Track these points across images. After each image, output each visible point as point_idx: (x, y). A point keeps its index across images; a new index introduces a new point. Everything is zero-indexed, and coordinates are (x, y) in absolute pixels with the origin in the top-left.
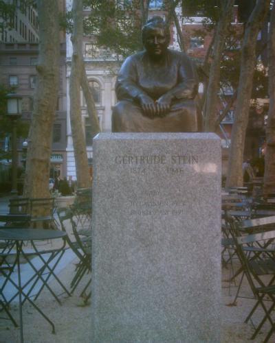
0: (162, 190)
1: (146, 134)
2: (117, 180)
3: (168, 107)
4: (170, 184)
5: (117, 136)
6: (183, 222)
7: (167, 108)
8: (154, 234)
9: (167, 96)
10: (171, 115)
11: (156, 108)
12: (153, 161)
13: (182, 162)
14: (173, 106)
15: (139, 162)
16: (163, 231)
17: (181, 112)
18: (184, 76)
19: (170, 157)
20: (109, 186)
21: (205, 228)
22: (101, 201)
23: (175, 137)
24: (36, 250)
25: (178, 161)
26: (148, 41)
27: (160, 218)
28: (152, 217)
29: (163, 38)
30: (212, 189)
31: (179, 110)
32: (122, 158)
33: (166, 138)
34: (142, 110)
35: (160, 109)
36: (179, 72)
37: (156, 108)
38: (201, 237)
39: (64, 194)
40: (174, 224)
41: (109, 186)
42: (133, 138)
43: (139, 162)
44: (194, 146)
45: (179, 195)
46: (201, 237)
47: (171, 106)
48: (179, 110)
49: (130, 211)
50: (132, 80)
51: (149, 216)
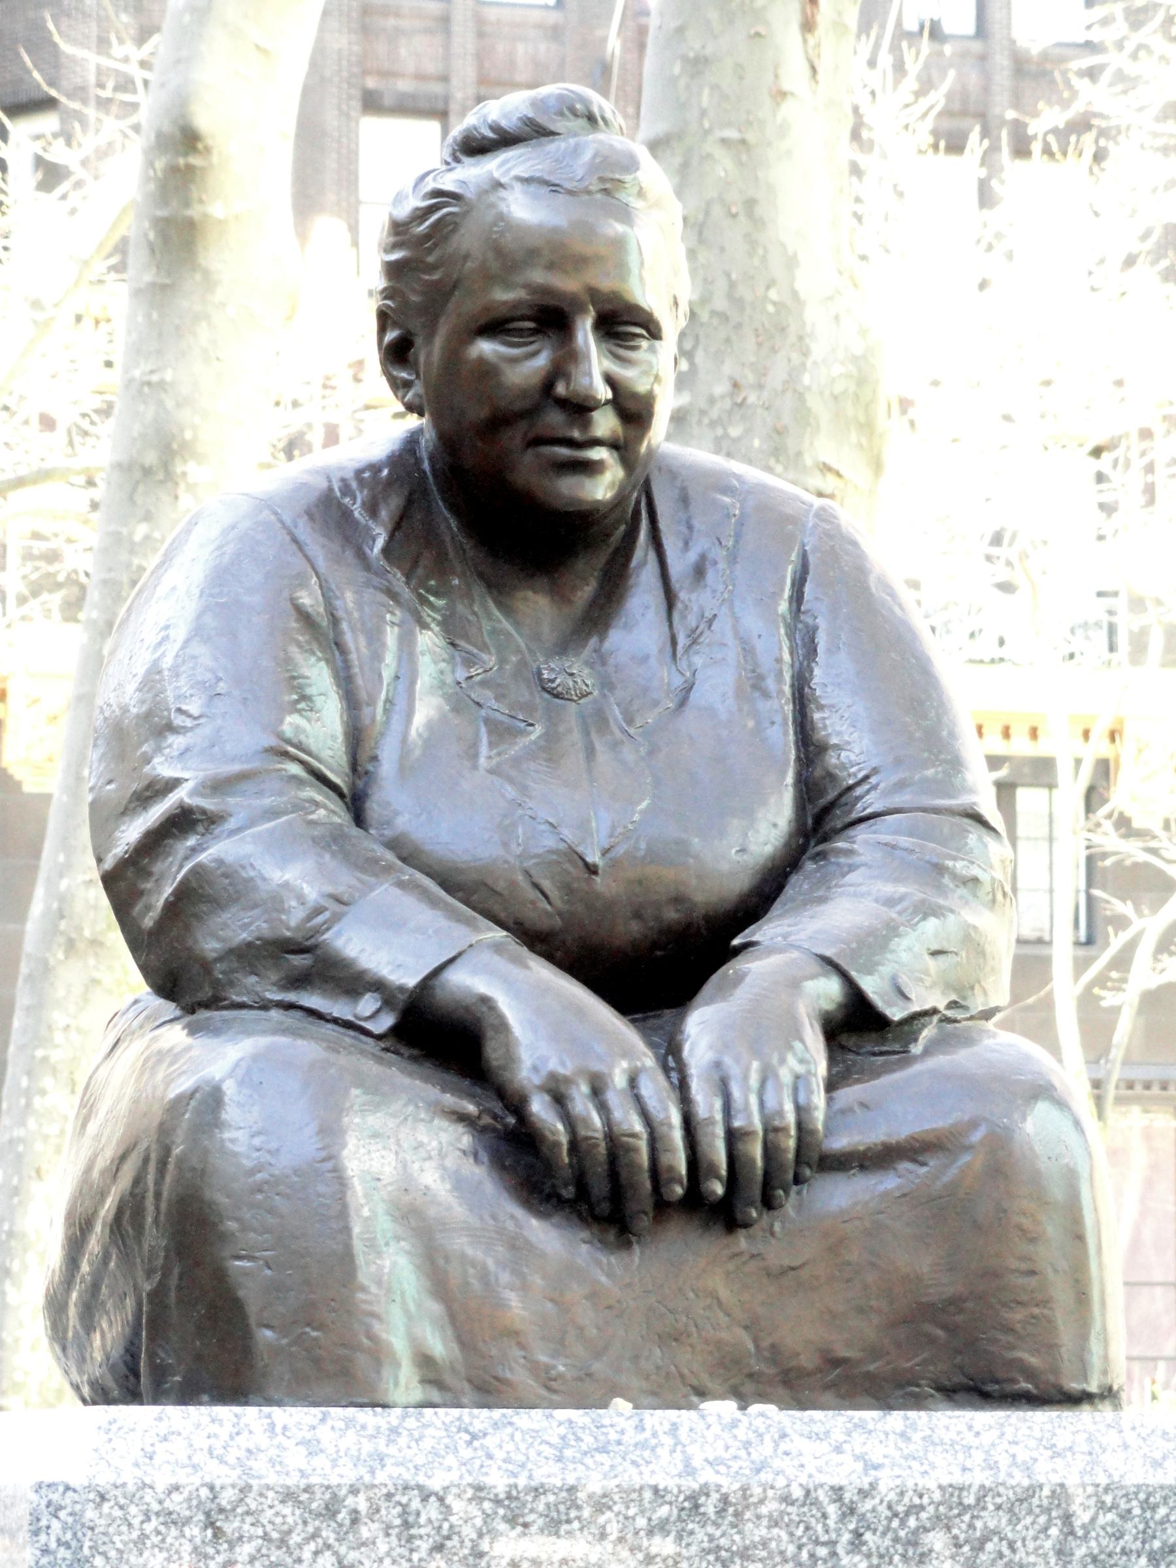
26: (486, 348)
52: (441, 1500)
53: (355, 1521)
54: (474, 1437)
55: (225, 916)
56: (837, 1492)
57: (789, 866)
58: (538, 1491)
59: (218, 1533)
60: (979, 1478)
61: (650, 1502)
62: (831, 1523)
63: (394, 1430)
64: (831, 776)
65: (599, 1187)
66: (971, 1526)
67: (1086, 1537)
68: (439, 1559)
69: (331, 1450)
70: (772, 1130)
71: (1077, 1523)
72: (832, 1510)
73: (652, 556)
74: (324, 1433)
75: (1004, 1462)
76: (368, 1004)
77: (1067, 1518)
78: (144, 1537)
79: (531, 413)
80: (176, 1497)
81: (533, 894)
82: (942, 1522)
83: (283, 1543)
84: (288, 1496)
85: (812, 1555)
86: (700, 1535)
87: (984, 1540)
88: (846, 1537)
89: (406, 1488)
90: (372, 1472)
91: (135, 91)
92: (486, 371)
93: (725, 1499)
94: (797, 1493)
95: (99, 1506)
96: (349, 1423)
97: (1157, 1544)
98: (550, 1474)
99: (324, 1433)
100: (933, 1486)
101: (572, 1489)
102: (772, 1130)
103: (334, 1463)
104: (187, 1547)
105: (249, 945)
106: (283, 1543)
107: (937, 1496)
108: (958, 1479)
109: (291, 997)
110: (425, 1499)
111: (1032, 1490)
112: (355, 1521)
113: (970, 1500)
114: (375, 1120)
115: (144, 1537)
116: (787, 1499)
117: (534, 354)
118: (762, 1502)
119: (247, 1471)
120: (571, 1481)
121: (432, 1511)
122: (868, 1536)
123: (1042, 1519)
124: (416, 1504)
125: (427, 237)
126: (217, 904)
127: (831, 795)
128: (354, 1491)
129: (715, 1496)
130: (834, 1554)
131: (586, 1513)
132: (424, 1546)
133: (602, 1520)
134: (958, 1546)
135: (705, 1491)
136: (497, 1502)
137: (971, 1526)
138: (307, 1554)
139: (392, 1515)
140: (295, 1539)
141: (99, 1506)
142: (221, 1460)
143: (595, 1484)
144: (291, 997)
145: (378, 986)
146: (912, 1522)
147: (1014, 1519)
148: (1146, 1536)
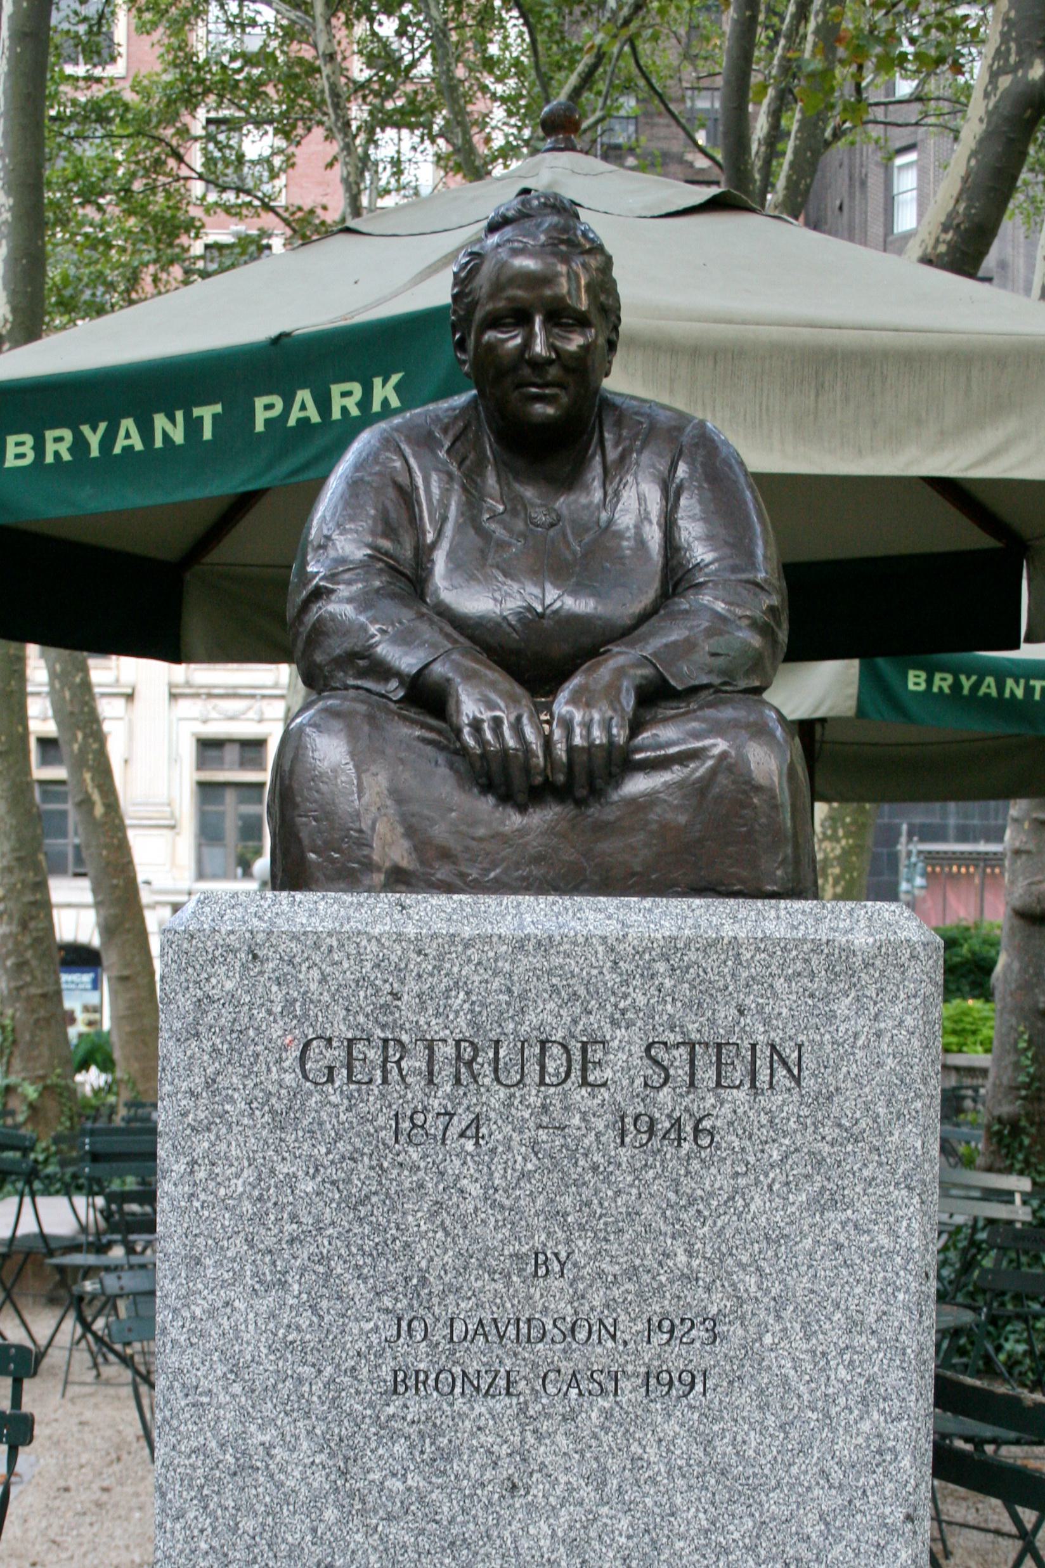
0: (583, 1245)
1: (489, 902)
2: (310, 1186)
3: (620, 734)
4: (633, 1214)
5: (626, 511)
6: (708, 1444)
7: (611, 742)
8: (530, 1507)
9: (605, 671)
10: (638, 785)
11: (548, 742)
12: (533, 1069)
13: (706, 1076)
14: (645, 736)
15: (445, 1074)
16: (587, 1493)
17: (699, 769)
18: (701, 553)
19: (638, 1050)
20: (259, 1218)
21: (837, 1475)
22: (212, 1313)
23: (668, 928)
24: (13, 1285)
25: (680, 1073)
26: (490, 336)
27: (568, 1418)
28: (523, 1409)
29: (582, 322)
30: (884, 1240)
31: (683, 758)
32: (337, 1054)
33: (612, 928)
34: (463, 751)
35: (571, 749)
36: (669, 526)
37: (548, 742)
38: (814, 1531)
39: (341, 534)
40: (652, 1453)
41: (259, 1218)
42: (411, 930)
43: (445, 1074)
44: (780, 984)
45: (689, 1278)
46: (814, 1531)
47: (636, 727)
48: (683, 758)
49: (386, 1372)
50: (395, 571)
51: (500, 1404)
52: (378, 940)
53: (330, 951)
54: (404, 908)
55: (331, 641)
56: (604, 939)
58: (434, 936)
59: (255, 957)
62: (600, 956)
63: (361, 905)
64: (681, 565)
66: (681, 960)
67: (749, 967)
69: (322, 913)
71: (744, 959)
72: (600, 949)
73: (599, 452)
75: (704, 924)
76: (394, 684)
78: (214, 958)
79: (515, 368)
80: (232, 937)
81: (509, 630)
84: (294, 937)
85: (588, 974)
86: (525, 961)
87: (688, 968)
88: (609, 964)
89: (359, 933)
90: (342, 925)
92: (491, 347)
93: (539, 943)
94: (581, 940)
95: (190, 942)
96: (335, 900)
97: (790, 971)
98: (441, 927)
100: (659, 936)
101: (453, 935)
103: (322, 921)
104: (238, 964)
105: (340, 656)
107: (662, 943)
109: (359, 683)
110: (369, 941)
111: (717, 941)
112: (330, 951)
113: (680, 945)
115: (214, 958)
116: (575, 943)
117: (515, 337)
118: (560, 944)
119: (273, 924)
120: (452, 931)
121: (374, 947)
122: (621, 964)
123: (723, 957)
124: (364, 943)
125: (466, 277)
126: (326, 634)
127: (680, 574)
128: (330, 934)
129: (533, 941)
130: (601, 973)
131: (460, 948)
132: (369, 965)
133: (469, 952)
134: (673, 970)
135: (528, 937)
136: (410, 941)
137: (681, 960)
138: (304, 969)
140: (297, 960)
141: (190, 942)
142: (260, 918)
143: (467, 932)
144: (359, 683)
145: (399, 675)
146: (647, 957)
148: (782, 966)
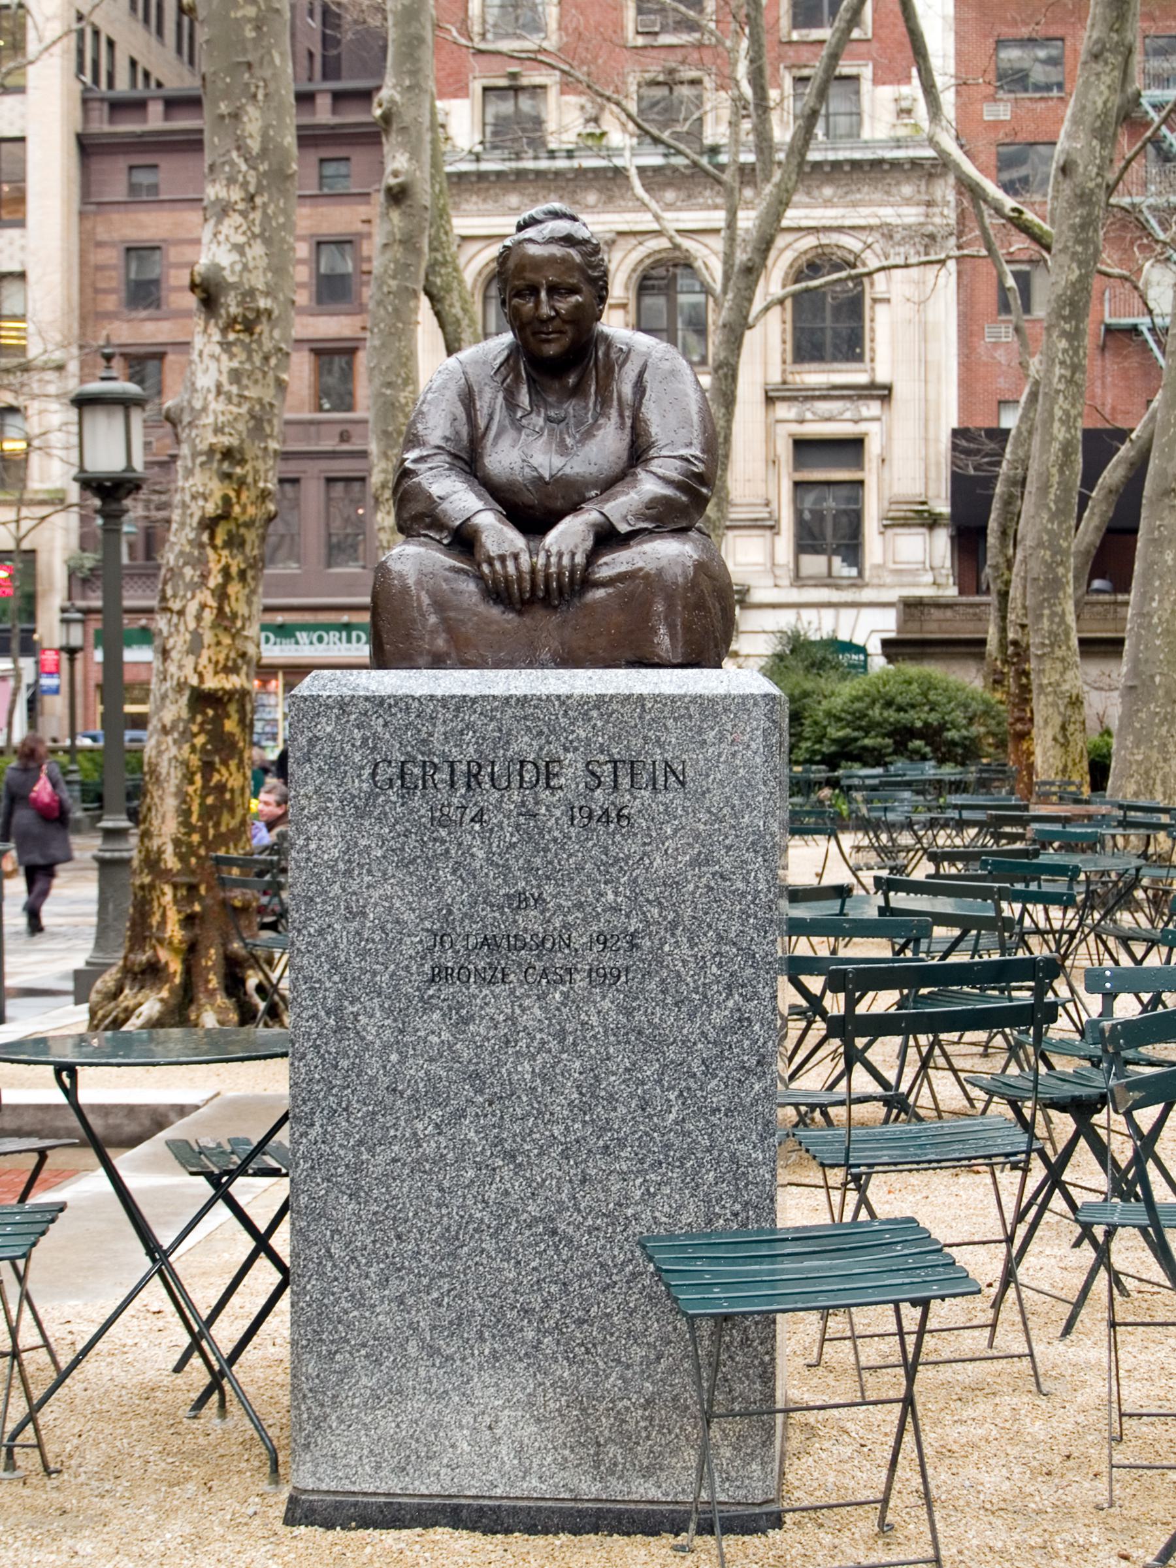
56: (558, 697)
57: (595, 486)
58: (453, 697)
60: (611, 692)
61: (829, 714)
65: (504, 595)
68: (1173, 762)
70: (560, 574)
74: (386, 679)
77: (643, 706)
82: (597, 707)
83: (365, 714)
84: (367, 699)
91: (641, 170)
99: (386, 679)
102: (547, 577)
106: (365, 714)
108: (604, 692)
114: (132, 592)
139: (403, 705)
147: (623, 706)
